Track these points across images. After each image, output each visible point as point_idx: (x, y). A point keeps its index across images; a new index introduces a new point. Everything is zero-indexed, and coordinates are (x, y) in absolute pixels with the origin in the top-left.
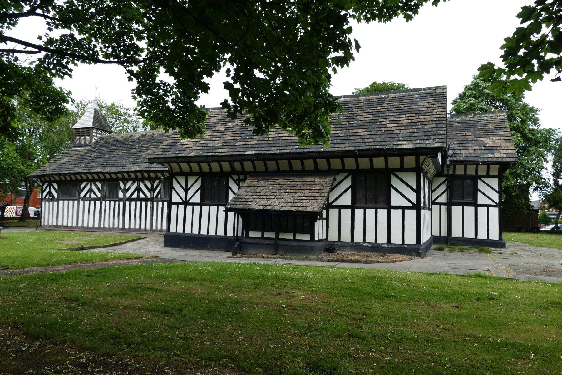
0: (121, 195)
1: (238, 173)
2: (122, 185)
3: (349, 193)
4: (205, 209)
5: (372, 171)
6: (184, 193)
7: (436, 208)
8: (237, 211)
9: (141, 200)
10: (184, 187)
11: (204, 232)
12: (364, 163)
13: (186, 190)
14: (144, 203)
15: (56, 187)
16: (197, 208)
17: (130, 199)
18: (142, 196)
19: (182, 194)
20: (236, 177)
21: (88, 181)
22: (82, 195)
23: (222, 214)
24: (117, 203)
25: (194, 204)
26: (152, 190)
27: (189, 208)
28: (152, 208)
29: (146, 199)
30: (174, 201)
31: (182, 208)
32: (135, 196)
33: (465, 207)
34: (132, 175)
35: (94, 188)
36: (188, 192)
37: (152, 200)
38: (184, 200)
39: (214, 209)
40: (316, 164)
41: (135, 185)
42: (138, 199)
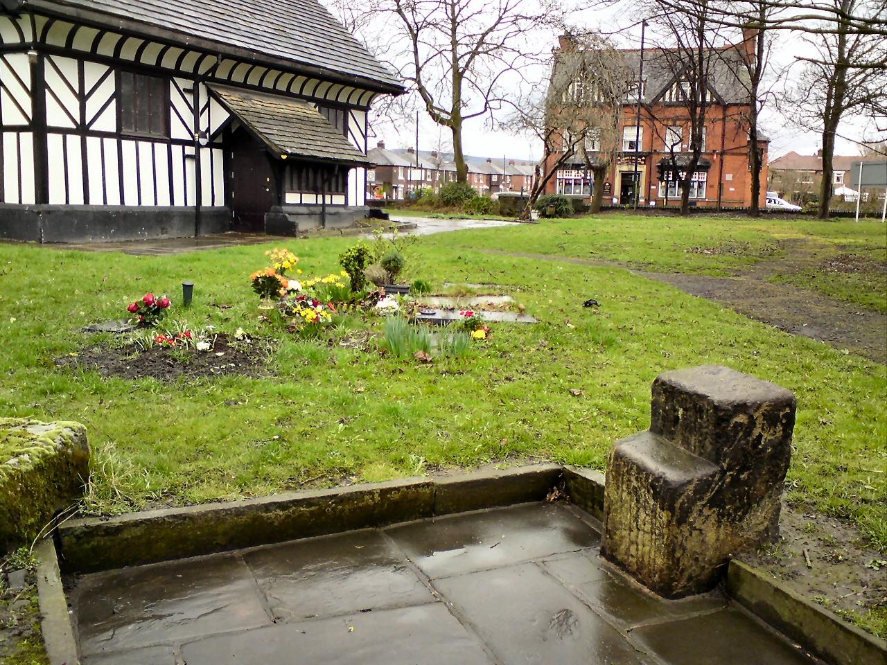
10: (77, 88)
13: (82, 98)
19: (73, 105)
25: (102, 135)
30: (51, 122)
31: (74, 141)
33: (21, 134)
36: (88, 103)
38: (79, 122)
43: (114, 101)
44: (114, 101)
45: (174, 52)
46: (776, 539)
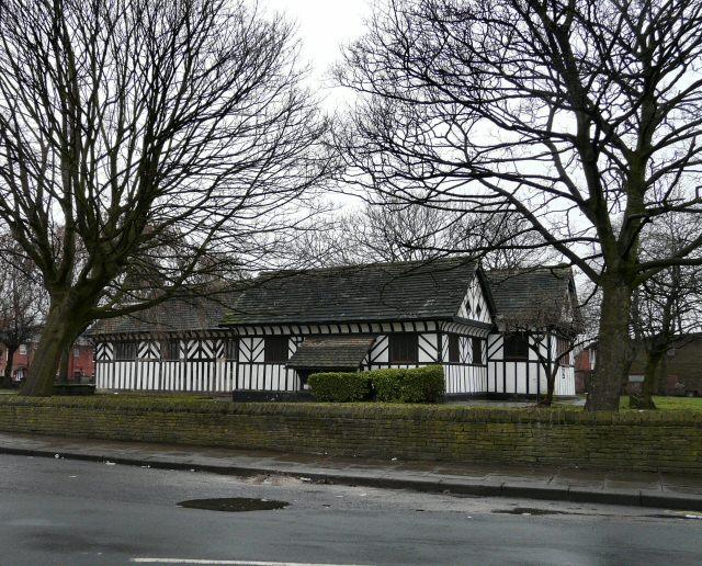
0: (182, 356)
1: (297, 336)
2: (182, 345)
3: (386, 352)
4: (269, 367)
5: (404, 334)
7: (491, 364)
8: (295, 368)
9: (203, 361)
11: (268, 388)
12: (398, 329)
14: (206, 364)
15: (112, 347)
16: (261, 367)
17: (192, 360)
18: (204, 356)
20: (294, 339)
21: (146, 341)
22: (140, 355)
23: (283, 372)
24: (178, 364)
25: (258, 364)
26: (214, 350)
27: (254, 367)
28: (215, 369)
29: (209, 360)
31: (248, 367)
32: (197, 356)
34: (194, 335)
35: (108, 351)
37: (214, 360)
39: (276, 367)
40: (370, 328)
41: (197, 345)
42: (200, 359)
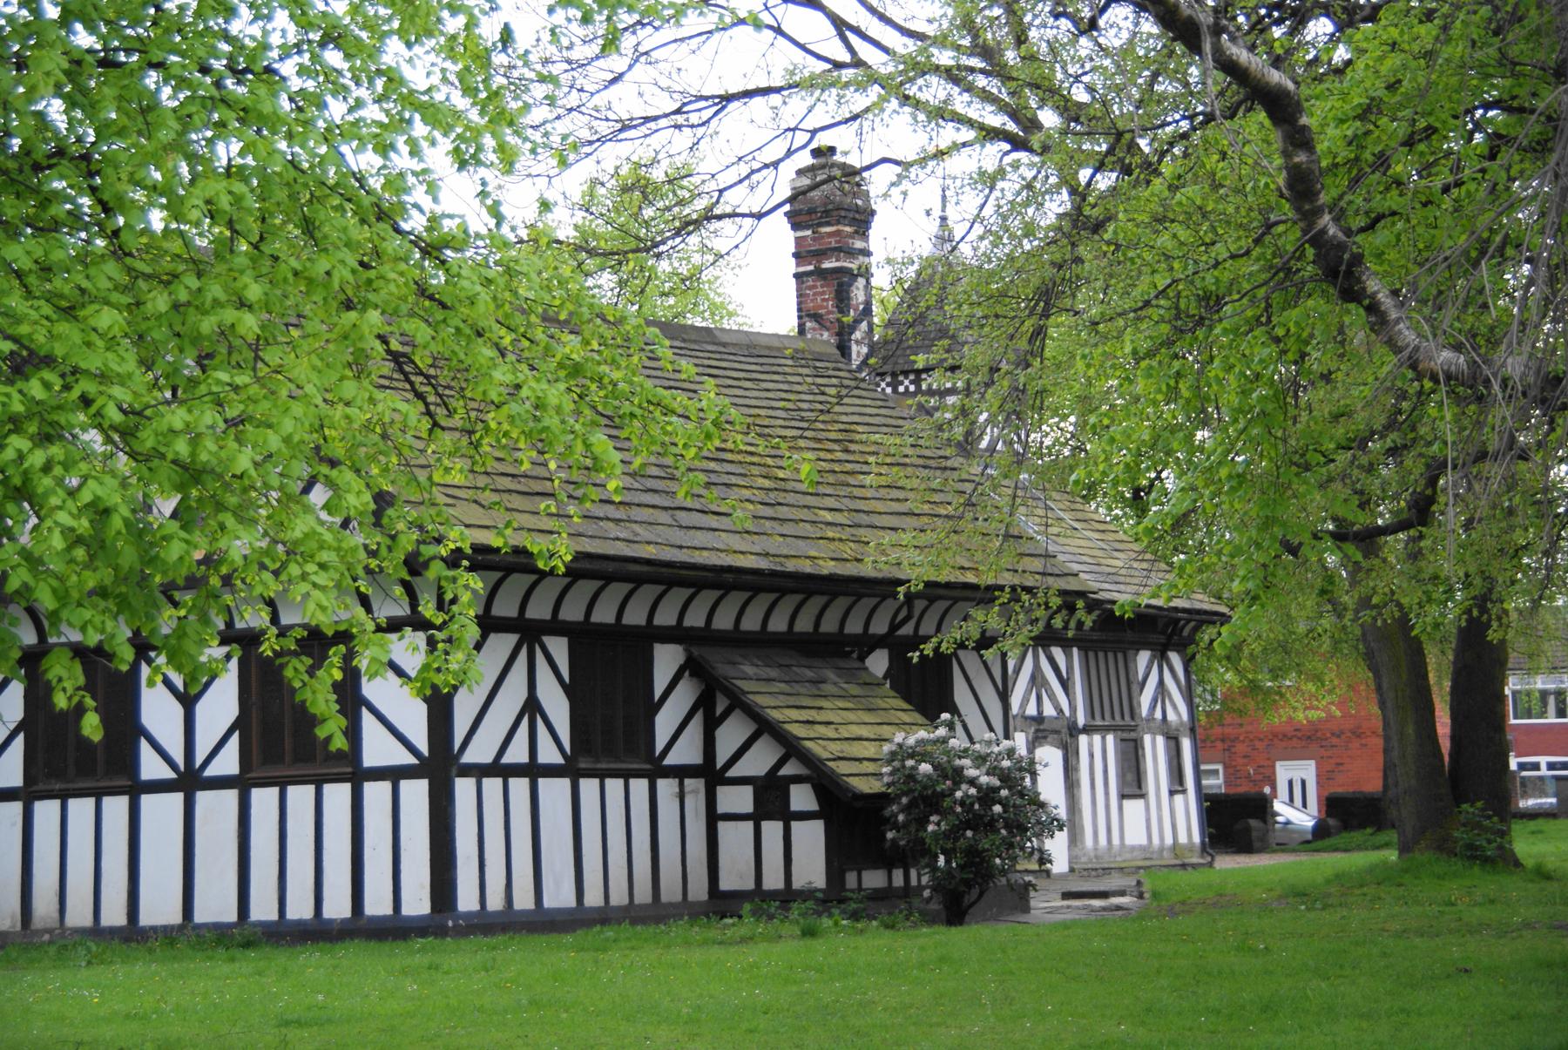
4: (264, 799)
6: (178, 710)
25: (681, 772)
36: (201, 708)
39: (81, 809)
43: (236, 735)
44: (236, 735)
45: (519, 582)
46: (99, 650)
